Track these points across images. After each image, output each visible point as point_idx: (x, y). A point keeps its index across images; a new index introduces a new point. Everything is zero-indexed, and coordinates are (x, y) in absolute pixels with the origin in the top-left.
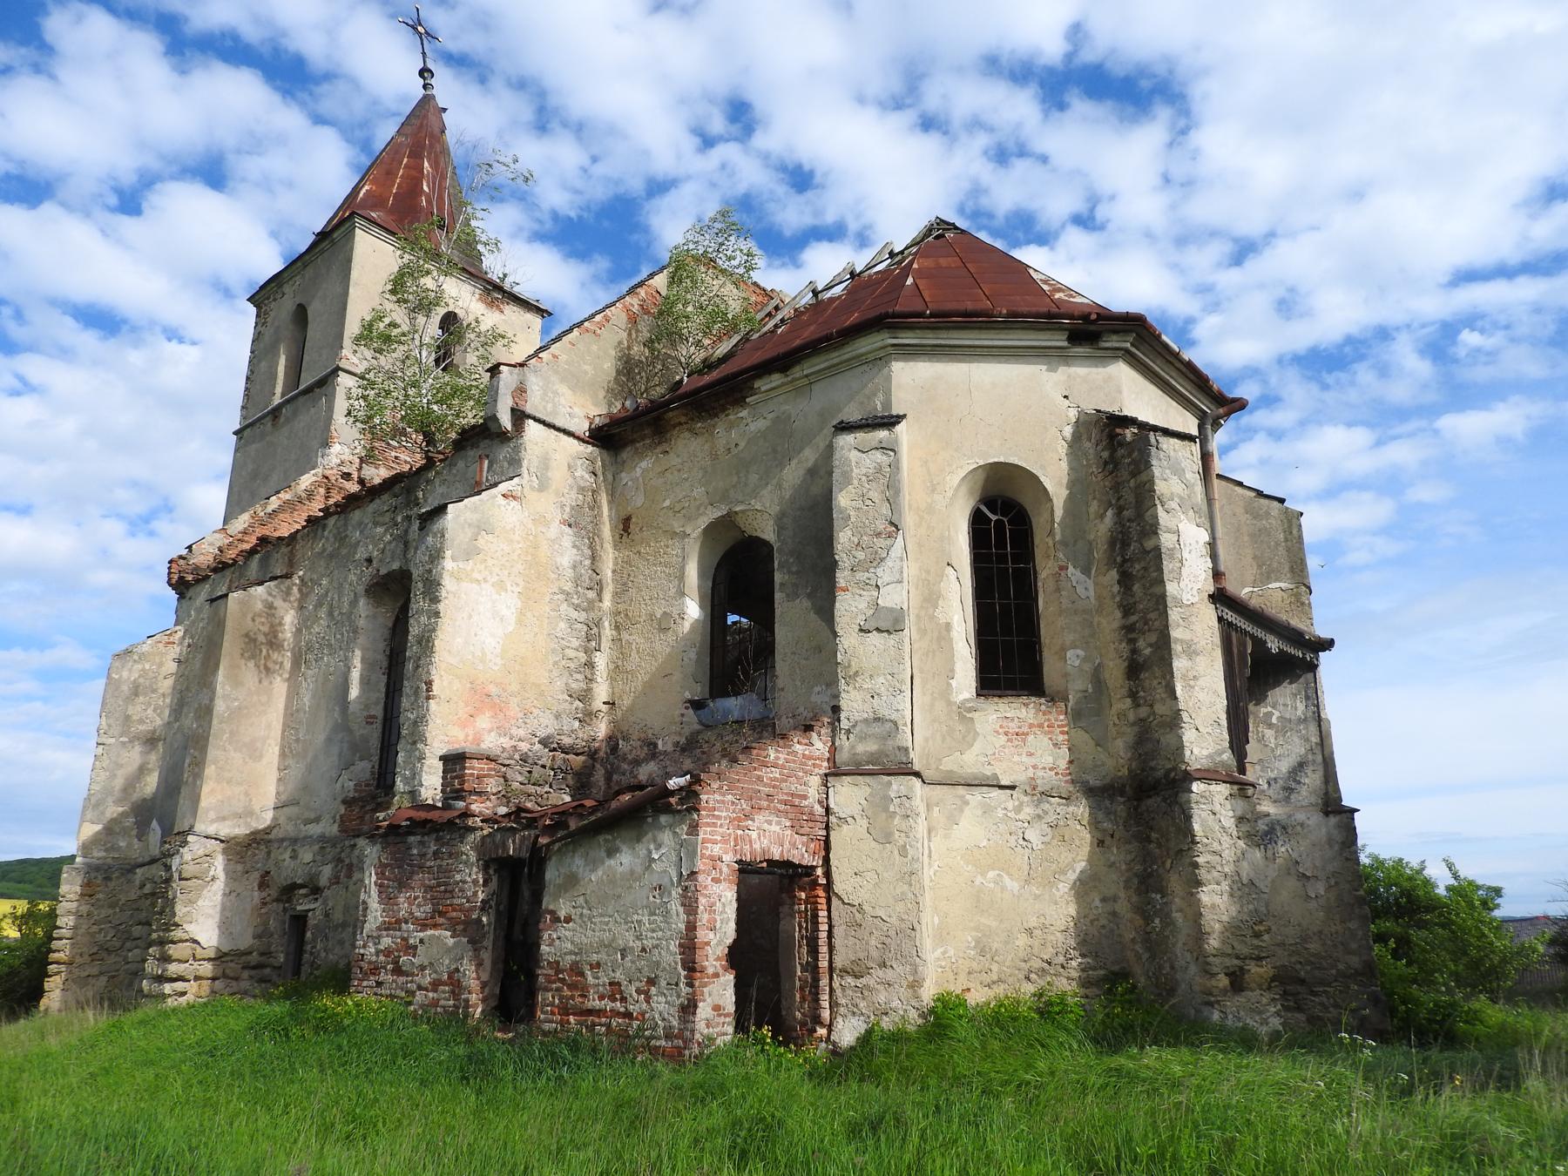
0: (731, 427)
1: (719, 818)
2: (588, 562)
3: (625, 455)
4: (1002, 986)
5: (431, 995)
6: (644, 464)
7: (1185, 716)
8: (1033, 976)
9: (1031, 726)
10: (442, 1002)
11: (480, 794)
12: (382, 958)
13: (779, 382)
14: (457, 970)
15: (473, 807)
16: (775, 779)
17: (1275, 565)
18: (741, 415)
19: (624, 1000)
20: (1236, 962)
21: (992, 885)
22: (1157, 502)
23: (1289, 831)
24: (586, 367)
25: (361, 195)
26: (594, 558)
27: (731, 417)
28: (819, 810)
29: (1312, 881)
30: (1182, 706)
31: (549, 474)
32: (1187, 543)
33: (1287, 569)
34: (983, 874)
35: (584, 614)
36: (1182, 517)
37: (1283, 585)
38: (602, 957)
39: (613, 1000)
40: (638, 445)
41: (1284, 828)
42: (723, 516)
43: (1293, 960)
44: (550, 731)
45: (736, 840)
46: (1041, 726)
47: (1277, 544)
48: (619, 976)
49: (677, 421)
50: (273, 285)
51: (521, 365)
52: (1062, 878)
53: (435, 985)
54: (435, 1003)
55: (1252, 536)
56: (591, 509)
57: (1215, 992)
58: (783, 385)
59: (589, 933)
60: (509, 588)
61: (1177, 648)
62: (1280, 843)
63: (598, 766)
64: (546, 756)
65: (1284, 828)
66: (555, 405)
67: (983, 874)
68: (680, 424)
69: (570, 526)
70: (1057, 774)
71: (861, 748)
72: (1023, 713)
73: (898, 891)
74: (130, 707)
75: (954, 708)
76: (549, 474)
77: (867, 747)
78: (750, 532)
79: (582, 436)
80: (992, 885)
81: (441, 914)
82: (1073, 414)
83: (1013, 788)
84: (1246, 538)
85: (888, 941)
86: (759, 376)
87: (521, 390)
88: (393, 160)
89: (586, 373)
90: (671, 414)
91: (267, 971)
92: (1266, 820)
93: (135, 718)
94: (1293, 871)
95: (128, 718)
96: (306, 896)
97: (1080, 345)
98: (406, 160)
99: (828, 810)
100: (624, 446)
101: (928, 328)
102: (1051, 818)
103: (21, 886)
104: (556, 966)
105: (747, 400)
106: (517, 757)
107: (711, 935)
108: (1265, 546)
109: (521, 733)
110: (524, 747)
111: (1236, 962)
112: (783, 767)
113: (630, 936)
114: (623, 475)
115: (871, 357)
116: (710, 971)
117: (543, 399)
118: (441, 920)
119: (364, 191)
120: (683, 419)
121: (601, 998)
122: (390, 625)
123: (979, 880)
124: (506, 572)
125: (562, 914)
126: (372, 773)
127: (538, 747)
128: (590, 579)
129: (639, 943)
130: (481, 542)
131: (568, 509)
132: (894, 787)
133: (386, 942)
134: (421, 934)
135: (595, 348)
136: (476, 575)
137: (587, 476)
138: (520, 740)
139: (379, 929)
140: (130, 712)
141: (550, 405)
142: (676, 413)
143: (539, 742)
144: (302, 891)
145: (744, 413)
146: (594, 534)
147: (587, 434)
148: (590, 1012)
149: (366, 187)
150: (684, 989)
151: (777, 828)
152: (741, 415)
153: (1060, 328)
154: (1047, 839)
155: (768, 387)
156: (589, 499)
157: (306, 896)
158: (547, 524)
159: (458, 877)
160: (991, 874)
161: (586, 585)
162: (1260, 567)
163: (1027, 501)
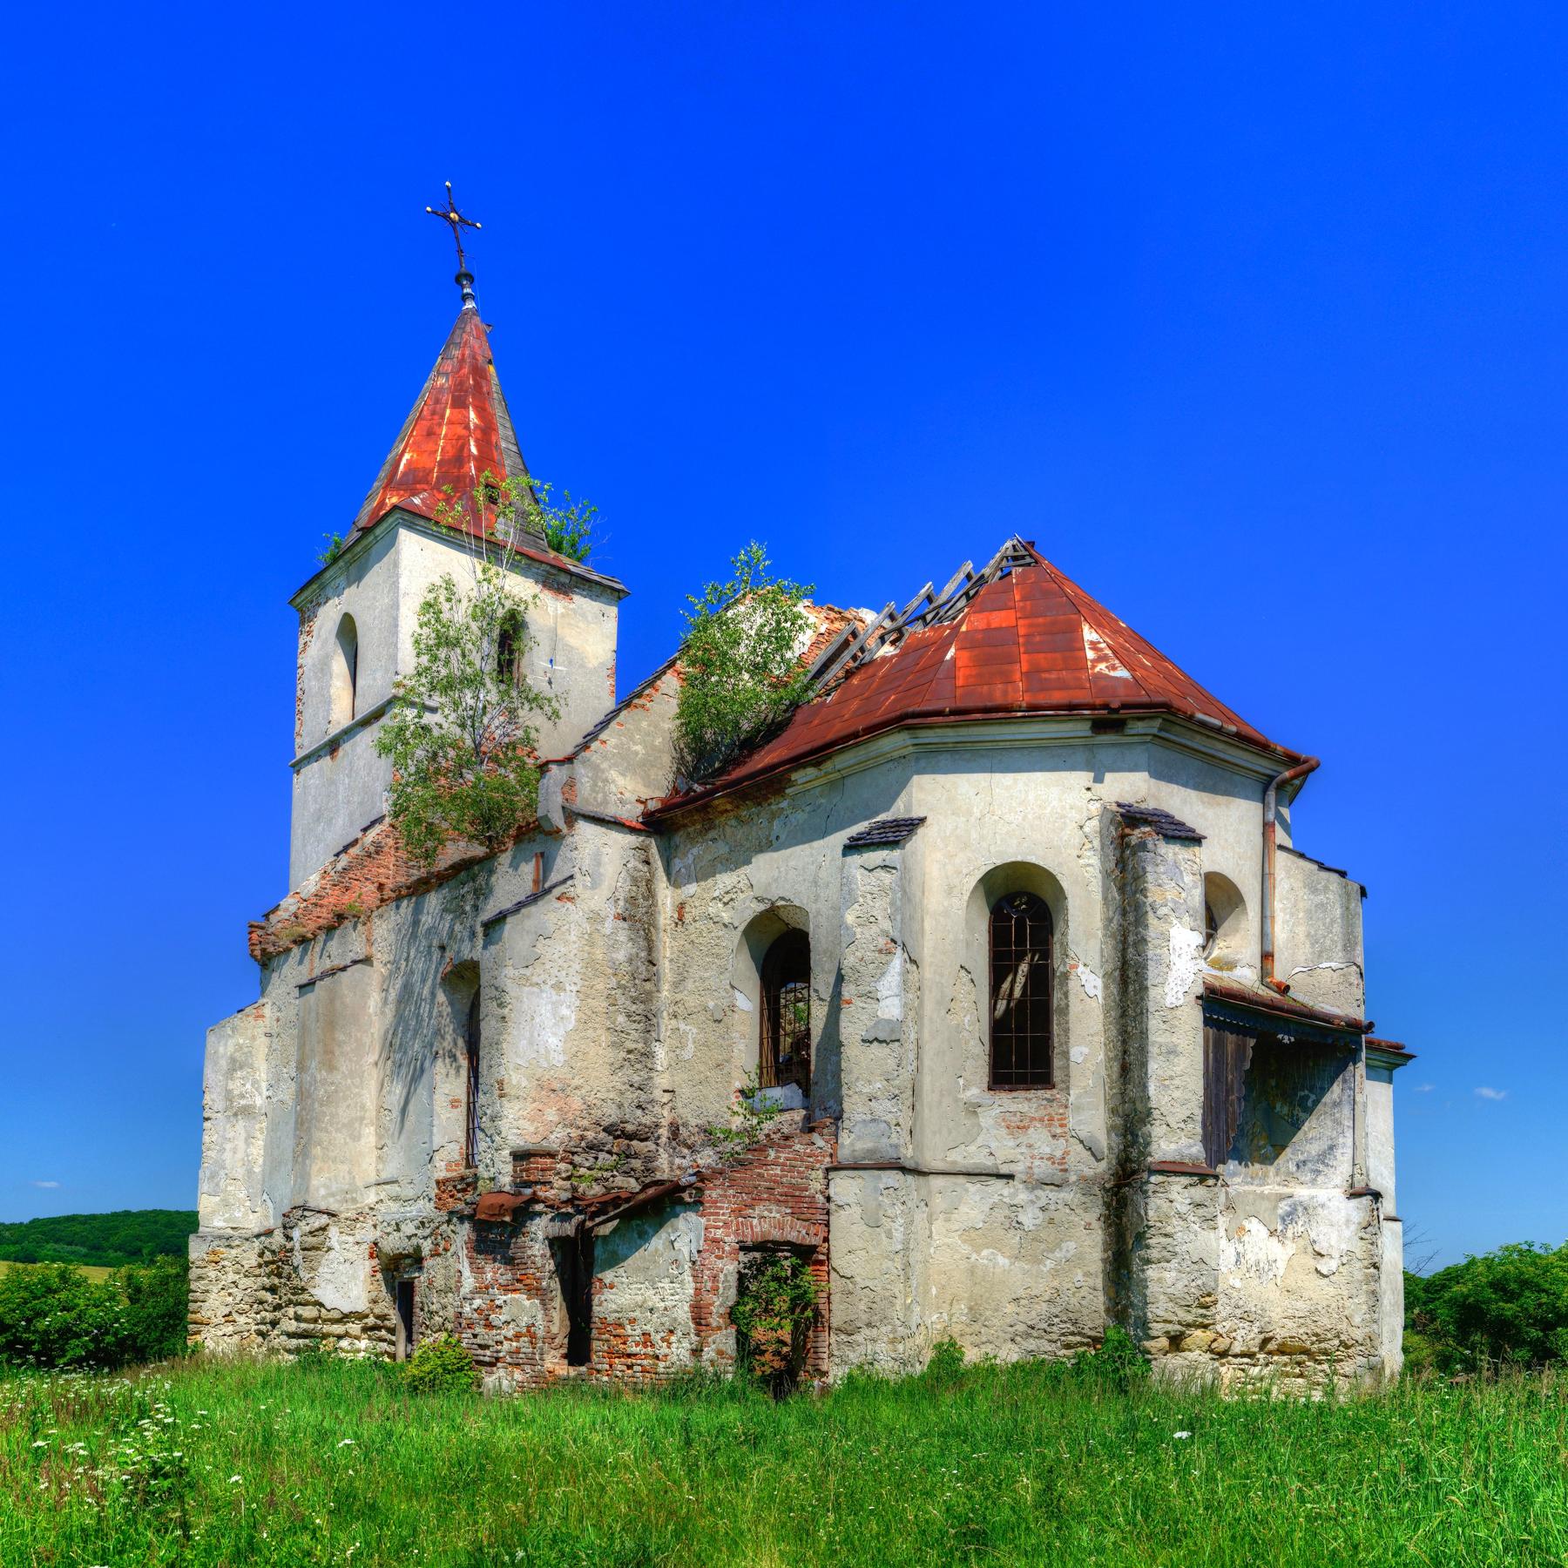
0: (773, 816)
1: (722, 1208)
2: (643, 954)
3: (678, 838)
4: (991, 1346)
5: (514, 1344)
6: (695, 851)
7: (1156, 1114)
8: (1018, 1339)
9: (1033, 1119)
10: (523, 1350)
11: (544, 1183)
12: (476, 1315)
13: (813, 776)
14: (533, 1325)
15: (540, 1193)
16: (776, 1175)
17: (1328, 942)
18: (781, 805)
19: (652, 1346)
20: (1178, 1327)
21: (985, 1262)
22: (1149, 909)
23: (1310, 1211)
24: (638, 748)
25: (402, 467)
26: (650, 949)
27: (773, 807)
28: (820, 1198)
29: (1326, 1259)
30: (1153, 1104)
31: (602, 870)
32: (1177, 948)
33: (1339, 947)
34: (978, 1253)
35: (643, 1006)
36: (1175, 921)
37: (1333, 965)
38: (637, 1314)
39: (646, 1347)
40: (691, 830)
41: (1305, 1209)
42: (767, 910)
43: (1301, 1331)
44: (613, 1119)
45: (737, 1225)
46: (1041, 1120)
47: (1333, 922)
48: (648, 1328)
49: (723, 808)
50: (314, 586)
51: (569, 760)
52: (1050, 1255)
53: (517, 1336)
54: (518, 1351)
55: (1308, 912)
56: (646, 899)
57: (1153, 1351)
58: (817, 778)
59: (627, 1296)
60: (568, 988)
61: (1153, 1050)
62: (1300, 1223)
63: (661, 1150)
64: (1115, 808)
65: (1305, 1209)
66: (605, 795)
67: (978, 1253)
68: (726, 811)
69: (624, 919)
70: (1053, 1163)
71: (859, 1146)
72: (1024, 1107)
73: (884, 1266)
74: (230, 1083)
75: (961, 1104)
76: (602, 870)
77: (863, 1145)
78: (793, 924)
79: (634, 824)
80: (985, 1262)
81: (519, 1281)
82: (1095, 808)
83: (1010, 1177)
84: (1301, 915)
85: (874, 1306)
86: (795, 769)
87: (571, 784)
88: (433, 413)
89: (636, 753)
90: (717, 802)
91: (383, 1332)
92: (1289, 1201)
93: (236, 1092)
94: (1310, 1249)
95: (229, 1092)
96: (411, 1265)
97: (1105, 733)
98: (448, 412)
99: (828, 1199)
100: (677, 830)
101: (948, 727)
102: (1043, 1202)
103: (73, 1248)
104: (603, 1320)
105: (788, 791)
106: (583, 1144)
107: (715, 1298)
108: (1320, 923)
109: (585, 1123)
110: (590, 1135)
111: (1178, 1327)
112: (783, 1165)
113: (656, 1299)
114: (677, 861)
115: (896, 754)
116: (714, 1324)
117: (593, 790)
118: (518, 1286)
119: (404, 461)
120: (729, 807)
121: (637, 1345)
122: (467, 1010)
123: (974, 1256)
124: (564, 973)
125: (607, 1281)
126: (461, 1154)
127: (603, 1135)
128: (647, 970)
129: (662, 1304)
130: (539, 949)
131: (621, 903)
132: (884, 1180)
133: (477, 1302)
134: (504, 1298)
135: (644, 724)
136: (535, 979)
137: (640, 866)
138: (585, 1129)
139: (471, 1292)
140: (231, 1086)
141: (600, 795)
142: (720, 801)
143: (604, 1130)
144: (408, 1261)
145: (784, 804)
146: (650, 924)
147: (640, 820)
148: (629, 1356)
149: (407, 456)
150: (694, 1338)
151: (778, 1216)
152: (781, 805)
153: (1083, 719)
154: (1038, 1222)
155: (805, 780)
156: (643, 889)
157: (411, 1265)
158: (603, 921)
159: (529, 1252)
160: (985, 1252)
161: (643, 977)
162: (1313, 945)
163: (1047, 896)
